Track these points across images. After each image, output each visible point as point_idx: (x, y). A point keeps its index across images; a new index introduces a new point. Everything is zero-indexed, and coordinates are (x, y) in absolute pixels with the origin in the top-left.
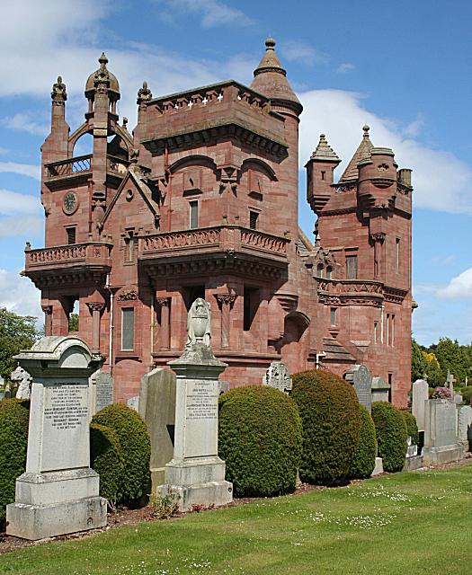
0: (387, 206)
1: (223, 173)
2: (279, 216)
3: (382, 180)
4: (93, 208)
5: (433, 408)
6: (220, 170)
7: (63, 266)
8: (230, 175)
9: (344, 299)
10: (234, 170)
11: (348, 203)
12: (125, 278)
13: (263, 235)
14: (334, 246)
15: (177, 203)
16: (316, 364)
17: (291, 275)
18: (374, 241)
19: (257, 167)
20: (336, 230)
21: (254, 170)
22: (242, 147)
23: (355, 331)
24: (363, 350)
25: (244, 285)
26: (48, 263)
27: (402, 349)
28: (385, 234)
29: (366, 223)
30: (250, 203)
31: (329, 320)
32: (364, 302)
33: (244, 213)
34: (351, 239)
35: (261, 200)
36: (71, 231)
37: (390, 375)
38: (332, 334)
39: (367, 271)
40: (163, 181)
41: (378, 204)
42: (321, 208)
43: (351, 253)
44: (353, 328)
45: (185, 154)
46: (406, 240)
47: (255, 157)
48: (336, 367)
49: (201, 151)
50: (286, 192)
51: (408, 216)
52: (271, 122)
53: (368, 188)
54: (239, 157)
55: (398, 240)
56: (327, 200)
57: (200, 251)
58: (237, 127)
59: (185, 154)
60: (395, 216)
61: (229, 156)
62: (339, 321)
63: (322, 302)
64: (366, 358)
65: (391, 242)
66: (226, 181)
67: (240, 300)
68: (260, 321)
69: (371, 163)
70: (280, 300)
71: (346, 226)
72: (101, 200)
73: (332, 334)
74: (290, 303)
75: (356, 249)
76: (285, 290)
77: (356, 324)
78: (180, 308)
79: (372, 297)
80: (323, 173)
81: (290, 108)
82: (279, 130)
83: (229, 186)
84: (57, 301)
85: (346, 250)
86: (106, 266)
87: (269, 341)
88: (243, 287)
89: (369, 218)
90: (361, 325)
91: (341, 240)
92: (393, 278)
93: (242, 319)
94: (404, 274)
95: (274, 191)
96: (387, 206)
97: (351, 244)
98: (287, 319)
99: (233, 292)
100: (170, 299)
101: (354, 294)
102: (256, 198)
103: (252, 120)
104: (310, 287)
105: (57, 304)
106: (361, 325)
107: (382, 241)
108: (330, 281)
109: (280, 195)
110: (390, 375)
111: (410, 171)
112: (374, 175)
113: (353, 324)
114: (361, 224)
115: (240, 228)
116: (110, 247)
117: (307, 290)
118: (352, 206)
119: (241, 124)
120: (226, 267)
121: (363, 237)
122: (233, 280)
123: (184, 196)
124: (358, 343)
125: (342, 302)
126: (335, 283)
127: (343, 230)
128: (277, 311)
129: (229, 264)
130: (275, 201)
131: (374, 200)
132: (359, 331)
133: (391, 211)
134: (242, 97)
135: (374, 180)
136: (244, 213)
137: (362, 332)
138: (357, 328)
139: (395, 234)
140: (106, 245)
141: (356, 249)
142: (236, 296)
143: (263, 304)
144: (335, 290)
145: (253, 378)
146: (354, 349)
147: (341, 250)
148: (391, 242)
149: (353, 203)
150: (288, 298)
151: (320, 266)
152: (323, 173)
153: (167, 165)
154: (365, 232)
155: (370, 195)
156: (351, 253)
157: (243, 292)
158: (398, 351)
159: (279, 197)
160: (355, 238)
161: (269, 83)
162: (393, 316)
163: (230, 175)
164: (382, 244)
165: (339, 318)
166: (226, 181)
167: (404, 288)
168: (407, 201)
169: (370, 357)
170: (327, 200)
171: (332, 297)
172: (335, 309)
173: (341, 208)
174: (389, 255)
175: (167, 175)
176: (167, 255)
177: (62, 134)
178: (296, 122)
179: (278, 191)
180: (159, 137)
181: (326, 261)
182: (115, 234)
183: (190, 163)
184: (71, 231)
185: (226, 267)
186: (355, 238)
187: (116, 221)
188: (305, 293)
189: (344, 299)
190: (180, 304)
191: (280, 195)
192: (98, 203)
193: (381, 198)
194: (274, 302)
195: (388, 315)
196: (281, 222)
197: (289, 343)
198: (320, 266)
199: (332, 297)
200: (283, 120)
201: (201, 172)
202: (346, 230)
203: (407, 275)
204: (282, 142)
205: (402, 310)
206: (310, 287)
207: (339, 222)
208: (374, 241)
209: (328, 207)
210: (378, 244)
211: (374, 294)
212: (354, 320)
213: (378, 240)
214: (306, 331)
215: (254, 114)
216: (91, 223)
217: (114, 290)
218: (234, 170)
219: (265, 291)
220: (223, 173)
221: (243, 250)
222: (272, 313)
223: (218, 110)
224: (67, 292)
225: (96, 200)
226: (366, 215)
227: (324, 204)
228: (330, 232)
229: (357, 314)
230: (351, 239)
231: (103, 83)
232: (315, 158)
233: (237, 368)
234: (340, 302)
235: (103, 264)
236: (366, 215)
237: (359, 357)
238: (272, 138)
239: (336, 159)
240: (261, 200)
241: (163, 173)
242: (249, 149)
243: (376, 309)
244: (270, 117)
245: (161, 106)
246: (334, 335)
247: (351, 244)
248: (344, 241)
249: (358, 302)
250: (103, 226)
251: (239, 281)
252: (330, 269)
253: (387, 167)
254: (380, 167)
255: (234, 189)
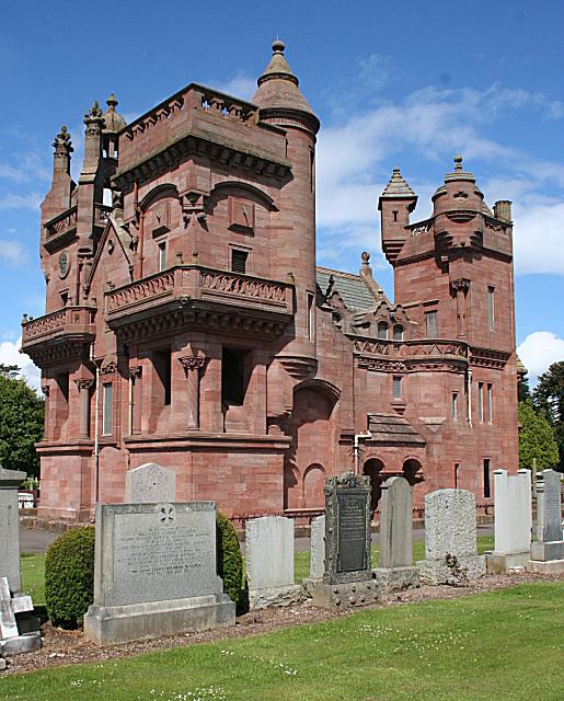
0: (468, 244)
1: (186, 201)
2: (282, 255)
3: (463, 212)
4: (81, 266)
5: (109, 525)
6: (182, 198)
7: (48, 338)
8: (193, 203)
9: (410, 364)
10: (199, 195)
11: (425, 246)
12: (106, 347)
13: (255, 281)
14: (407, 302)
15: (149, 246)
16: (354, 448)
17: (299, 331)
18: (456, 291)
19: (243, 193)
20: (413, 282)
21: (238, 197)
22: (211, 167)
23: (425, 404)
24: (434, 429)
25: (223, 344)
26: (40, 334)
27: (504, 426)
28: (469, 281)
29: (444, 268)
30: (232, 239)
31: (391, 392)
32: (435, 367)
33: (222, 252)
34: (430, 290)
35: (253, 235)
36: (65, 297)
37: (486, 462)
38: (396, 410)
39: (450, 329)
40: (134, 222)
41: (456, 243)
42: (395, 256)
43: (430, 306)
44: (423, 401)
45: (153, 185)
46: (505, 288)
47: (236, 179)
48: (391, 452)
49: (165, 179)
50: (291, 225)
51: (509, 259)
52: (260, 135)
53: (445, 225)
54: (206, 179)
55: (491, 289)
56: (402, 245)
57: (155, 303)
58: (198, 141)
59: (153, 185)
60: (484, 258)
61: (192, 177)
62: (406, 392)
63: (365, 367)
64: (439, 438)
65: (479, 291)
66: (190, 212)
67: (216, 365)
68: (253, 394)
69: (445, 193)
70: (283, 363)
71: (424, 275)
72: (89, 257)
73: (396, 410)
74: (304, 367)
75: (436, 302)
76: (291, 350)
77: (427, 396)
78: (151, 379)
79: (446, 361)
80: (395, 213)
81: (295, 119)
82: (275, 145)
83: (194, 217)
84: (53, 380)
85: (425, 305)
86: (86, 335)
87: (268, 418)
88: (221, 347)
89: (447, 262)
90: (434, 397)
91: (419, 293)
92: (486, 336)
93: (220, 388)
94: (503, 331)
95: (273, 224)
96: (468, 244)
97: (430, 297)
98: (297, 391)
99: (201, 354)
100: (141, 368)
101: (421, 356)
102: (243, 233)
103: (226, 133)
104: (340, 348)
105: (53, 383)
106: (434, 397)
107: (466, 290)
108: (390, 342)
109: (281, 228)
110: (486, 462)
111: (509, 203)
112: (449, 206)
113: (423, 394)
114: (440, 271)
115: (197, 268)
116: (94, 311)
117: (335, 352)
118: (429, 249)
119: (204, 136)
120: (186, 321)
121: (443, 286)
122: (203, 339)
123: (154, 237)
124: (428, 420)
125: (409, 369)
126: (397, 345)
127: (420, 280)
128: (280, 378)
129: (188, 317)
130: (276, 236)
131: (451, 238)
132: (430, 405)
133: (478, 251)
134: (229, 111)
135: (450, 213)
136: (222, 252)
137: (435, 406)
138: (428, 400)
139: (485, 280)
140: (87, 308)
141: (436, 302)
142: (207, 360)
143: (258, 370)
144: (398, 355)
145: (242, 468)
146: (424, 429)
147: (416, 306)
148: (479, 291)
149: (430, 246)
150: (295, 361)
151: (383, 325)
152: (395, 213)
153: (138, 204)
154: (445, 280)
155: (446, 233)
156: (430, 306)
157: (221, 354)
158: (500, 430)
159: (280, 231)
160: (435, 289)
161: (269, 92)
162: (490, 386)
163: (193, 203)
164: (466, 293)
165: (406, 389)
166: (190, 212)
167: (508, 350)
168: (504, 239)
169: (447, 437)
170: (402, 245)
171: (394, 362)
172: (400, 378)
173: (417, 253)
174: (478, 307)
175: (137, 214)
176: (128, 312)
177: (63, 189)
178: (479, 198)
179: (279, 224)
180: (126, 170)
181: (392, 319)
182: (99, 289)
183: (161, 195)
184: (65, 297)
185: (186, 321)
186: (435, 289)
187: (100, 280)
188: (329, 355)
189: (410, 364)
190: (150, 374)
191: (281, 228)
192: (85, 261)
193: (461, 235)
194: (275, 368)
195: (481, 385)
196: (283, 262)
197: (312, 421)
198: (383, 325)
199: (394, 362)
200: (284, 133)
201: (168, 204)
202: (427, 280)
203: (509, 332)
204: (281, 159)
205: (503, 377)
206: (340, 348)
207: (416, 271)
208: (456, 291)
209: (404, 254)
210: (460, 294)
211: (449, 356)
212: (423, 391)
213: (460, 289)
214: (337, 405)
215: (230, 125)
216: (79, 285)
217: (99, 362)
218: (199, 195)
219: (259, 353)
220: (186, 201)
221: (204, 297)
222: (272, 384)
223: (179, 122)
224: (61, 369)
225: (83, 257)
226: (444, 258)
227: (399, 251)
228: (407, 285)
229: (426, 387)
230: (430, 290)
231: (93, 122)
232: (386, 195)
233: (208, 454)
234: (405, 369)
235: (83, 332)
236: (444, 258)
237: (429, 438)
238: (262, 155)
239: (411, 195)
240: (253, 235)
241: (133, 213)
242: (224, 169)
243: (456, 375)
244: (259, 129)
245: (131, 133)
246: (400, 411)
247: (430, 297)
248: (422, 293)
249: (428, 367)
250: (89, 287)
251: (213, 339)
252: (399, 329)
253: (466, 196)
254: (456, 196)
255: (202, 221)
